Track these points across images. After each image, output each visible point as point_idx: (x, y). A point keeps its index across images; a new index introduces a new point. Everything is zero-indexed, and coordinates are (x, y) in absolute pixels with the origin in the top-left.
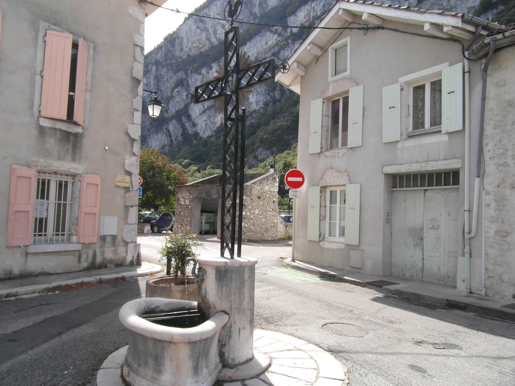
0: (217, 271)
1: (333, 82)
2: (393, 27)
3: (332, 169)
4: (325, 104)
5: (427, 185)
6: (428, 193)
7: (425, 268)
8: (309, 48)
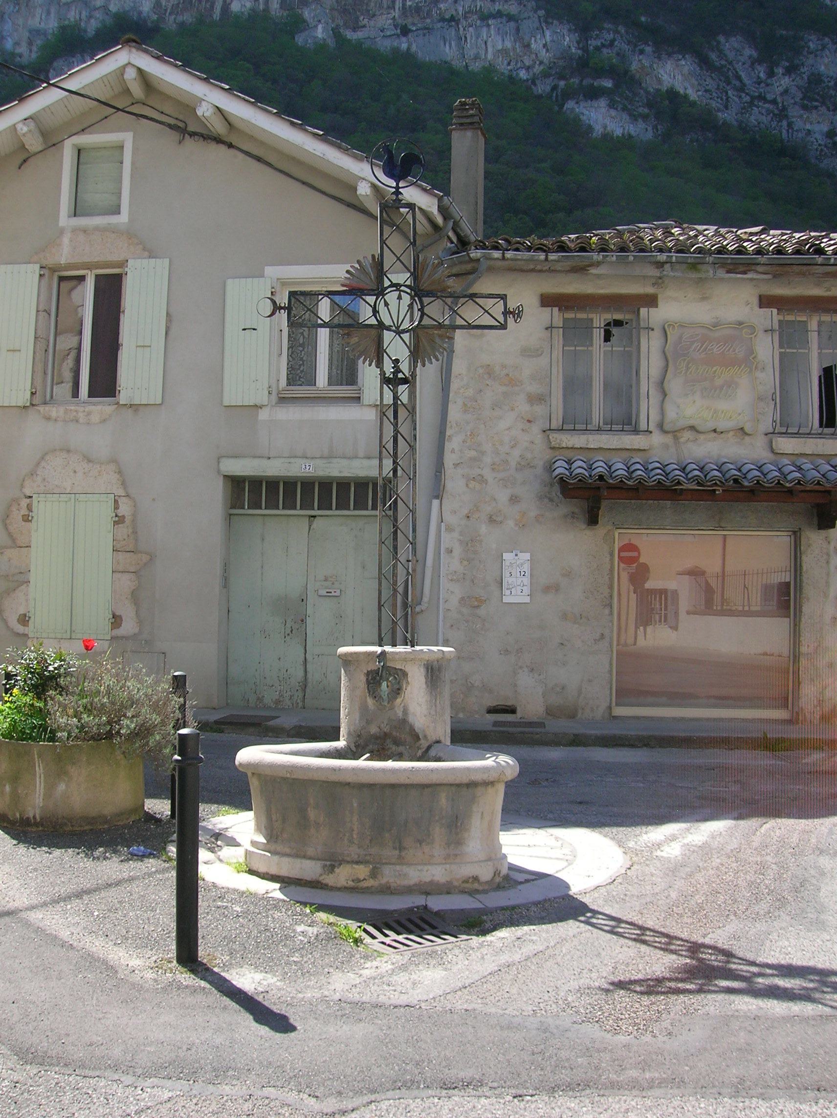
0: (427, 669)
1: (75, 230)
2: (255, 152)
3: (68, 451)
4: (45, 280)
5: (281, 506)
6: (317, 523)
7: (310, 680)
8: (25, 129)
